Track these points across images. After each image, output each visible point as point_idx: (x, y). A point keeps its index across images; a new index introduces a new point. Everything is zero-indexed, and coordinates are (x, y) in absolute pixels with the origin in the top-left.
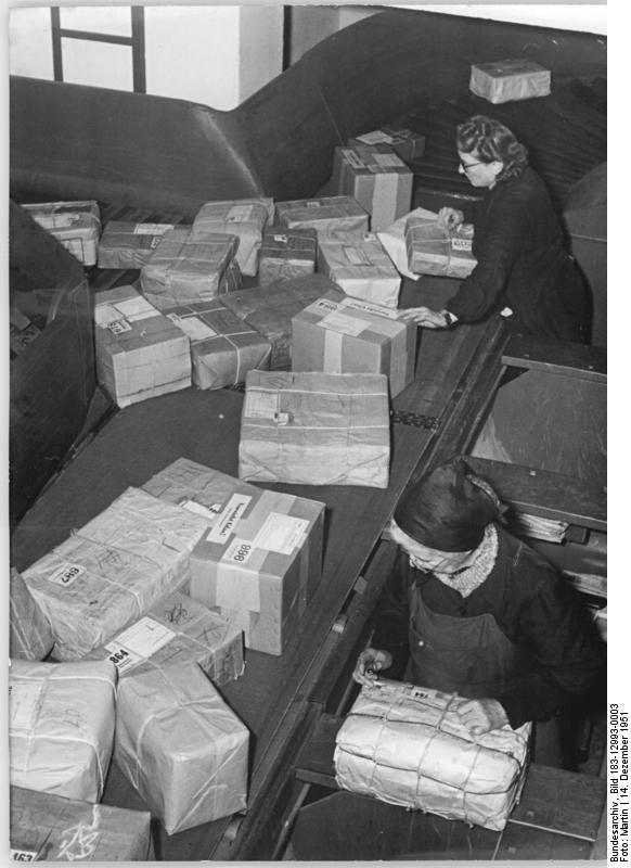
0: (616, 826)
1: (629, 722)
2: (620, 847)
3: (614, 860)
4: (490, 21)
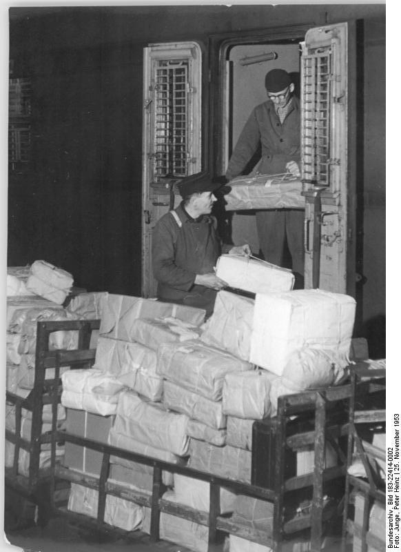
1: (400, 421)
2: (394, 539)
3: (390, 547)
4: (348, 132)
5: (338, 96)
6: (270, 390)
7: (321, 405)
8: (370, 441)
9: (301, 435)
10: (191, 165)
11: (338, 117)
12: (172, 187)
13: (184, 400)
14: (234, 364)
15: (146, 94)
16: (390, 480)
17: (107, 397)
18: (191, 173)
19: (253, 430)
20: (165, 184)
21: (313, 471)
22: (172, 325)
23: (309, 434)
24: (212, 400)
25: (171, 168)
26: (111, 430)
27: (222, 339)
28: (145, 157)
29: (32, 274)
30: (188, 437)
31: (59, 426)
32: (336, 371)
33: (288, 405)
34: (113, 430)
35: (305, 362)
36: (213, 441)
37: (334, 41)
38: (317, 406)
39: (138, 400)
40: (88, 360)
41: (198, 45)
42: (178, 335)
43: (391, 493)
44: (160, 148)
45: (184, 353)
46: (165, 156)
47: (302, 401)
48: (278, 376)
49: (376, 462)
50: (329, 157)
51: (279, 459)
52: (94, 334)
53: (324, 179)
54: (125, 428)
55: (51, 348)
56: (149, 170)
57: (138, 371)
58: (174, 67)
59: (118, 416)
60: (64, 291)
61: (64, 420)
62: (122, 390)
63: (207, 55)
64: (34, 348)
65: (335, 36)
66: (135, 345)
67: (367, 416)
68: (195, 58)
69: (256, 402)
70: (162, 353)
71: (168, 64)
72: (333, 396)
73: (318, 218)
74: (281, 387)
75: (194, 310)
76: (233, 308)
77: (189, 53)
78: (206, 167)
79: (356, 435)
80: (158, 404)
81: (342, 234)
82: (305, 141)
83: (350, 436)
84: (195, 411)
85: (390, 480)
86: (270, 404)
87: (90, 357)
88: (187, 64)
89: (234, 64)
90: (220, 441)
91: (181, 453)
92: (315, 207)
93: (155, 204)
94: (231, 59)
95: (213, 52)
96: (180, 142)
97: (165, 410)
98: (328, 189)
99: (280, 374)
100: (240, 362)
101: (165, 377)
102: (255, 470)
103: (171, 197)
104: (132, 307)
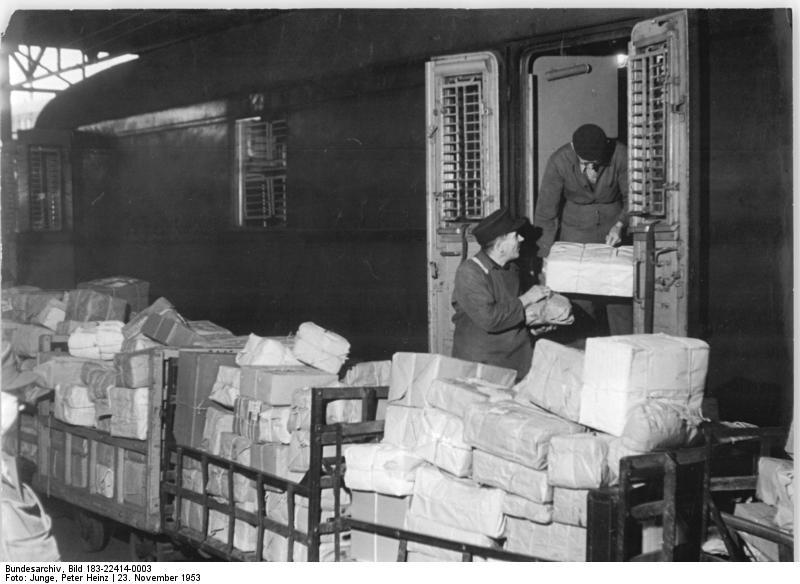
0: (39, 570)
2: (19, 574)
3: (8, 568)
5: (677, 103)
6: (607, 453)
7: (672, 468)
8: (731, 511)
9: (647, 504)
10: (488, 205)
11: (677, 131)
12: (464, 233)
13: (500, 472)
14: (561, 425)
15: (430, 120)
16: (105, 569)
17: (402, 474)
18: (488, 213)
19: (589, 502)
20: (455, 229)
21: (660, 548)
22: (480, 385)
23: (657, 504)
24: (534, 469)
25: (463, 210)
26: (408, 512)
27: (544, 397)
28: (430, 198)
29: (300, 338)
30: (504, 515)
31: (343, 512)
32: (688, 428)
33: (632, 468)
34: (411, 513)
35: (652, 418)
36: (536, 519)
37: (671, 33)
38: (666, 471)
39: (440, 476)
40: (375, 433)
41: (490, 53)
42: (488, 396)
43: (85, 569)
44: (451, 186)
45: (497, 414)
46: (455, 196)
47: (647, 464)
48: (617, 437)
49: (739, 536)
50: (665, 180)
51: (622, 532)
52: (381, 403)
53: (657, 208)
54: (425, 511)
55: (329, 422)
56: (435, 212)
57: (438, 441)
58: (464, 84)
59: (415, 497)
60: (338, 357)
61: (348, 505)
62: (419, 465)
63: (504, 67)
64: (309, 422)
65: (672, 28)
66: (434, 410)
67: (726, 484)
68: (490, 71)
70: (471, 415)
71: (456, 80)
72: (686, 459)
73: (651, 257)
74: (621, 448)
75: (501, 370)
76: (557, 359)
77: (483, 66)
78: (506, 204)
79: (712, 505)
80: (465, 480)
81: (682, 275)
82: (633, 164)
83: (705, 507)
84: (513, 483)
85: (105, 569)
86: (608, 469)
87: (380, 430)
88: (481, 80)
89: (539, 78)
90: (545, 518)
91: (496, 535)
92: (648, 245)
93: (444, 254)
94: (535, 72)
95: (512, 64)
97: (473, 486)
98: (663, 221)
99: (619, 435)
100: (566, 423)
101: (474, 445)
102: (591, 548)
104: (427, 366)
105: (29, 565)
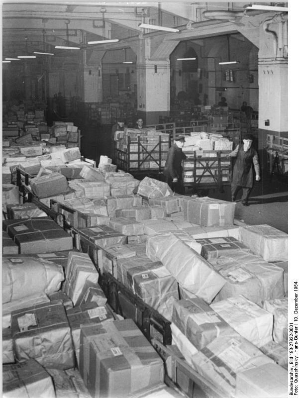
0: (292, 379)
1: (298, 287)
2: (294, 388)
3: (291, 394)
16: (291, 346)
43: (291, 356)
69: (61, 344)
85: (291, 346)
96: (155, 204)
103: (63, 209)
105: (289, 384)
